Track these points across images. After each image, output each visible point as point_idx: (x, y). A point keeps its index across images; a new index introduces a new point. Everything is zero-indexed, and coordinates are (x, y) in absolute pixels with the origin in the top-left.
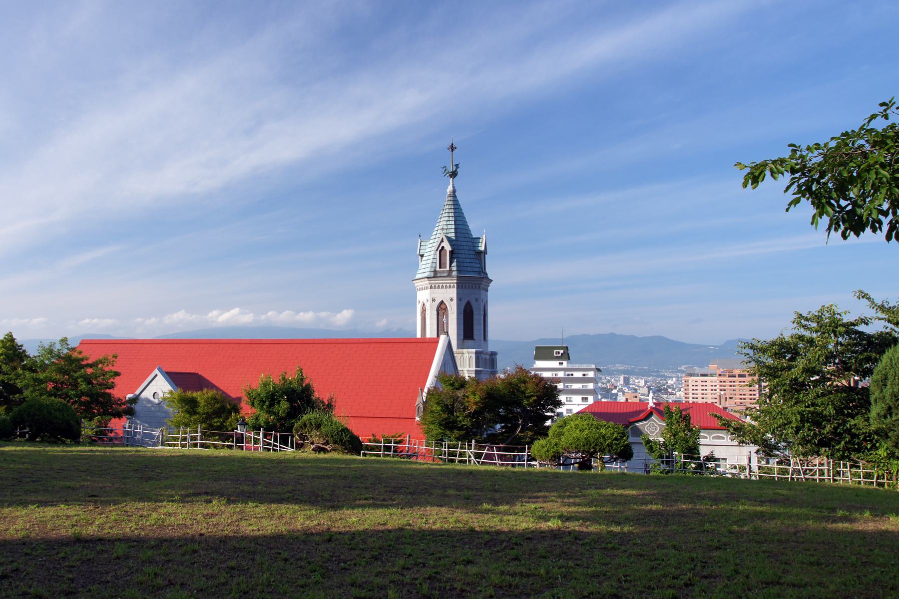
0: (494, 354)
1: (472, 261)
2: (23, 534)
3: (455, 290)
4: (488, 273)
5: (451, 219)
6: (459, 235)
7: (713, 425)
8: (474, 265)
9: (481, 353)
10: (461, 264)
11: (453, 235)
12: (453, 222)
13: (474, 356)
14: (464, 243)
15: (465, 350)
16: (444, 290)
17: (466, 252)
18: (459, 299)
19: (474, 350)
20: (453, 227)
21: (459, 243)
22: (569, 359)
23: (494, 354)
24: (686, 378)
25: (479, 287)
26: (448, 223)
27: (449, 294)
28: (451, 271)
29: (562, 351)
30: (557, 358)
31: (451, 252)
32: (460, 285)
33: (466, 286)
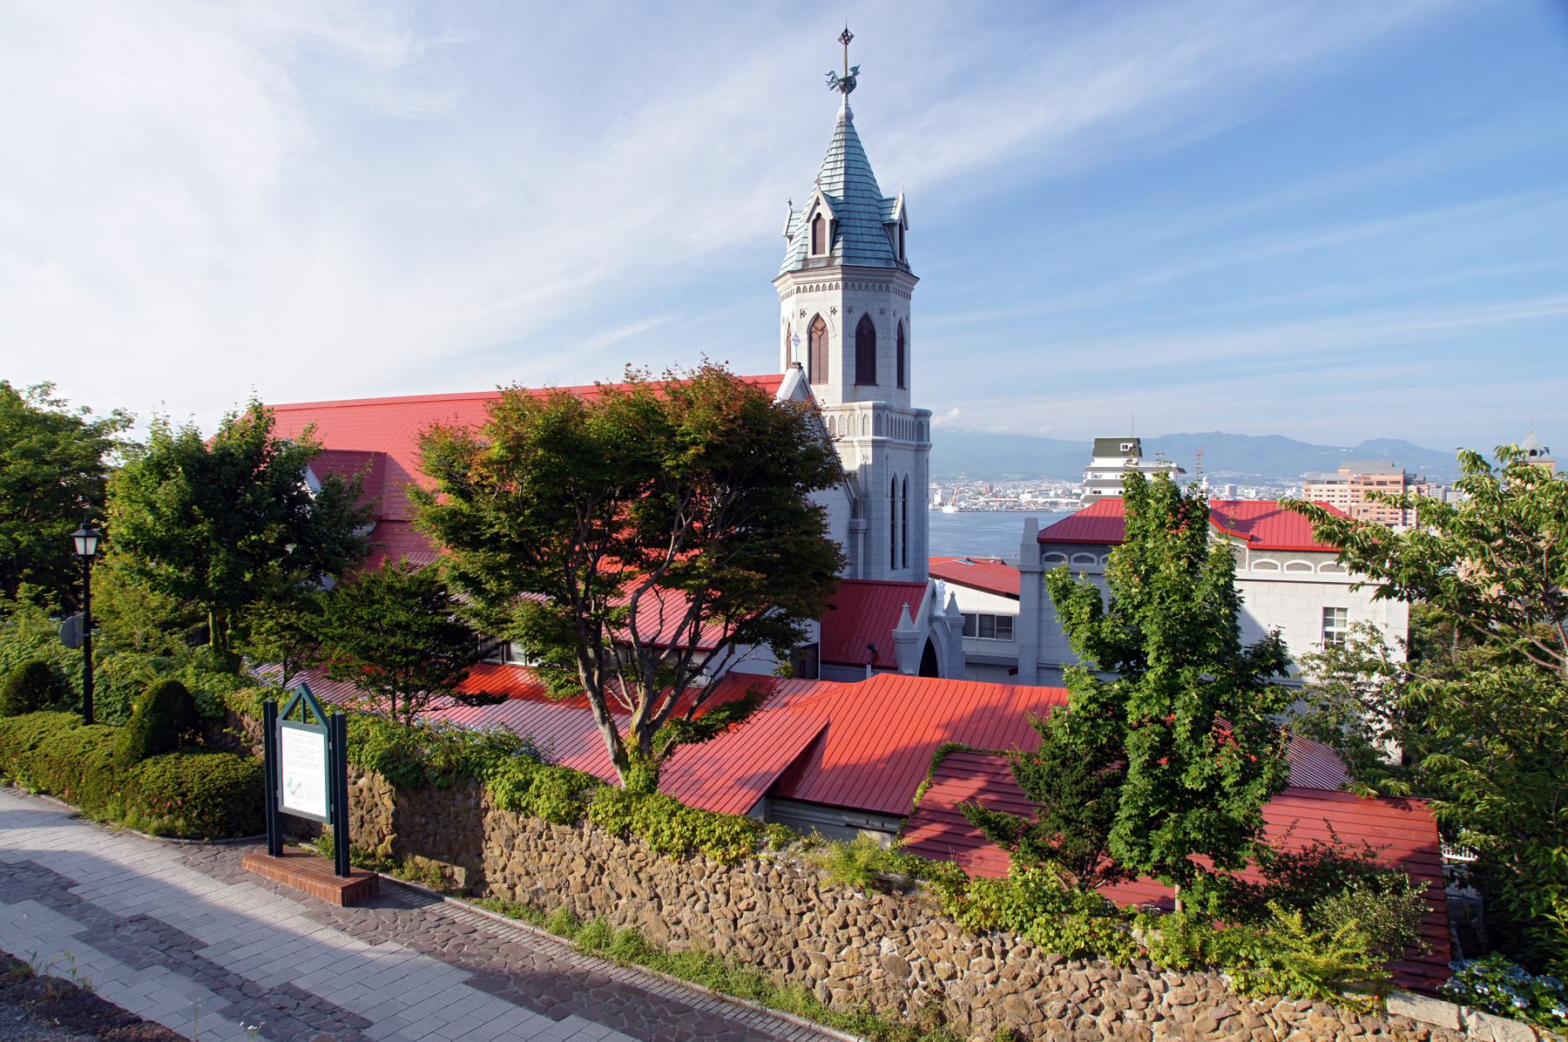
0: (923, 415)
1: (875, 239)
3: (839, 293)
4: (910, 264)
5: (839, 165)
6: (851, 193)
7: (1281, 544)
8: (877, 247)
9: (884, 408)
10: (852, 245)
11: (841, 193)
12: (842, 171)
13: (870, 413)
14: (861, 208)
15: (856, 405)
16: (820, 293)
17: (864, 223)
18: (848, 310)
19: (870, 403)
20: (842, 178)
21: (851, 207)
22: (1141, 455)
23: (923, 415)
24: (1308, 487)
25: (887, 287)
26: (834, 173)
27: (829, 301)
28: (832, 257)
29: (1130, 445)
30: (1124, 454)
31: (835, 224)
32: (850, 284)
33: (853, 285)
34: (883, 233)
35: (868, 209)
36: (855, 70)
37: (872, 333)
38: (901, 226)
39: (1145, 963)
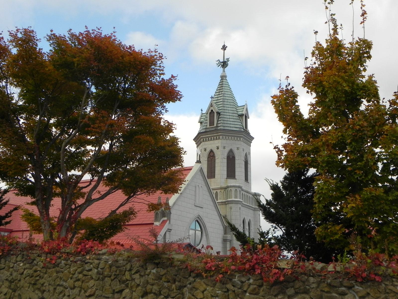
2: (197, 265)
4: (250, 133)
8: (236, 123)
17: (230, 114)
26: (219, 96)
34: (238, 118)
35: (232, 109)
36: (228, 59)
37: (234, 158)
38: (246, 117)
39: (209, 249)
